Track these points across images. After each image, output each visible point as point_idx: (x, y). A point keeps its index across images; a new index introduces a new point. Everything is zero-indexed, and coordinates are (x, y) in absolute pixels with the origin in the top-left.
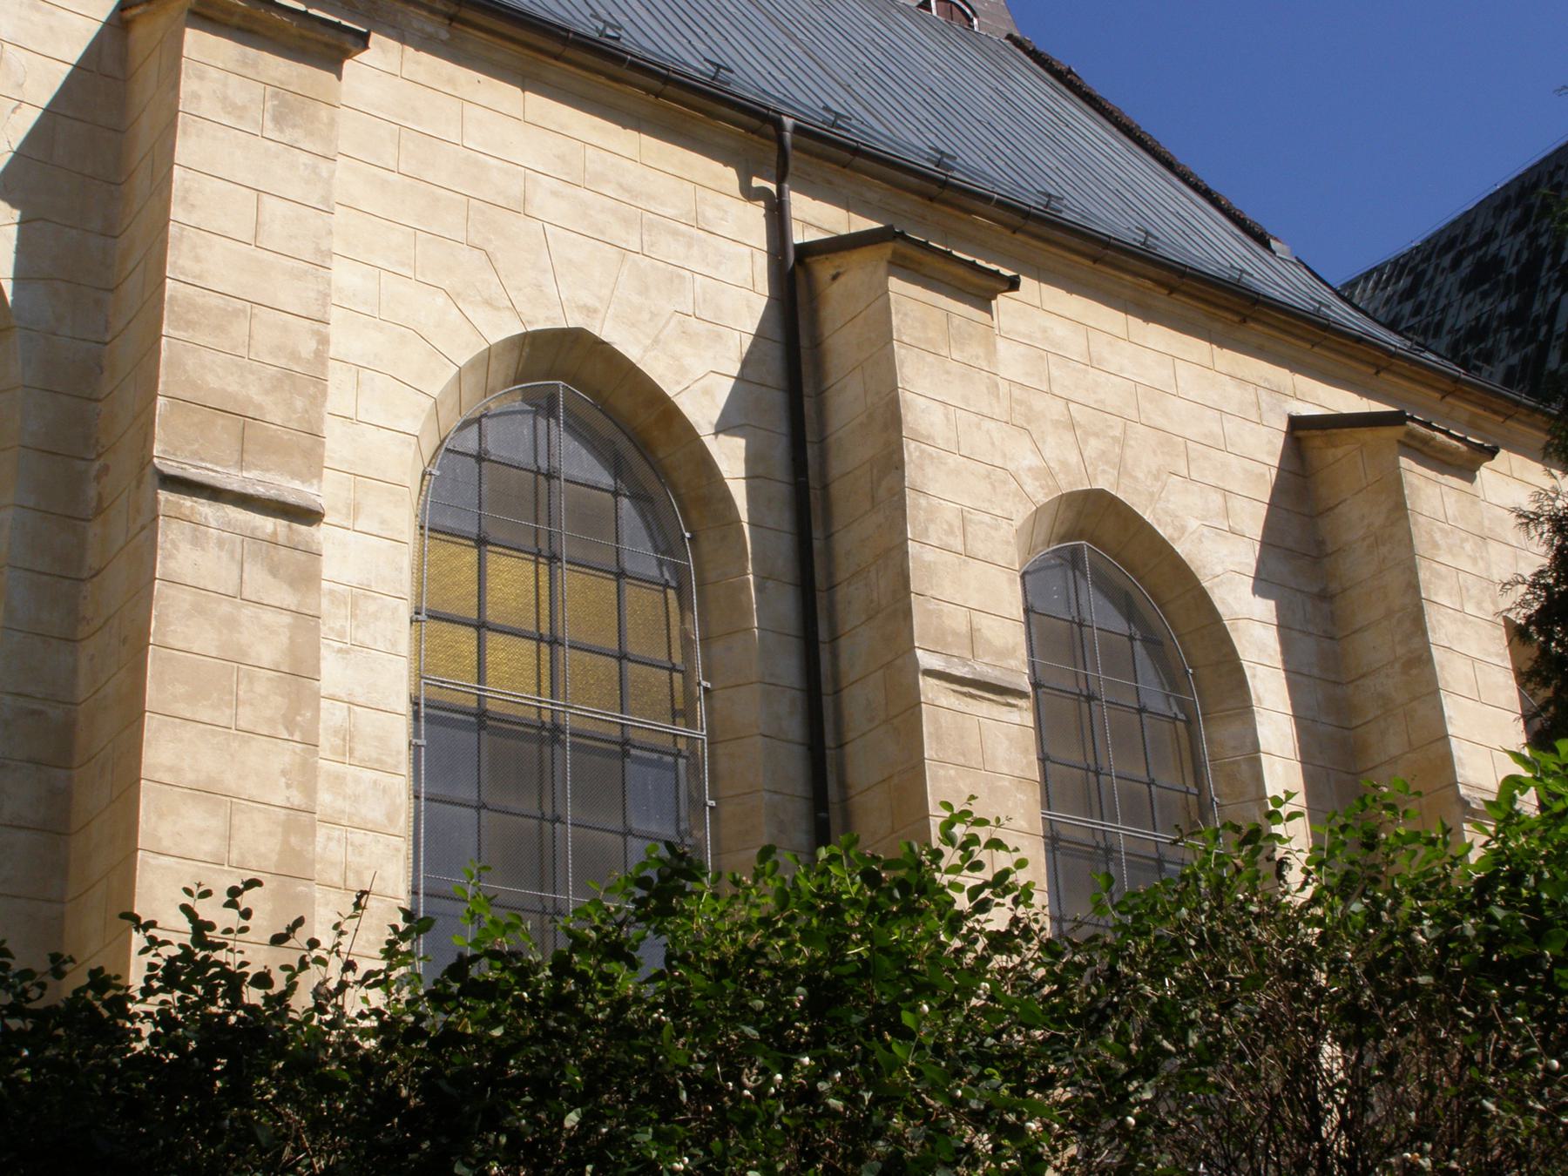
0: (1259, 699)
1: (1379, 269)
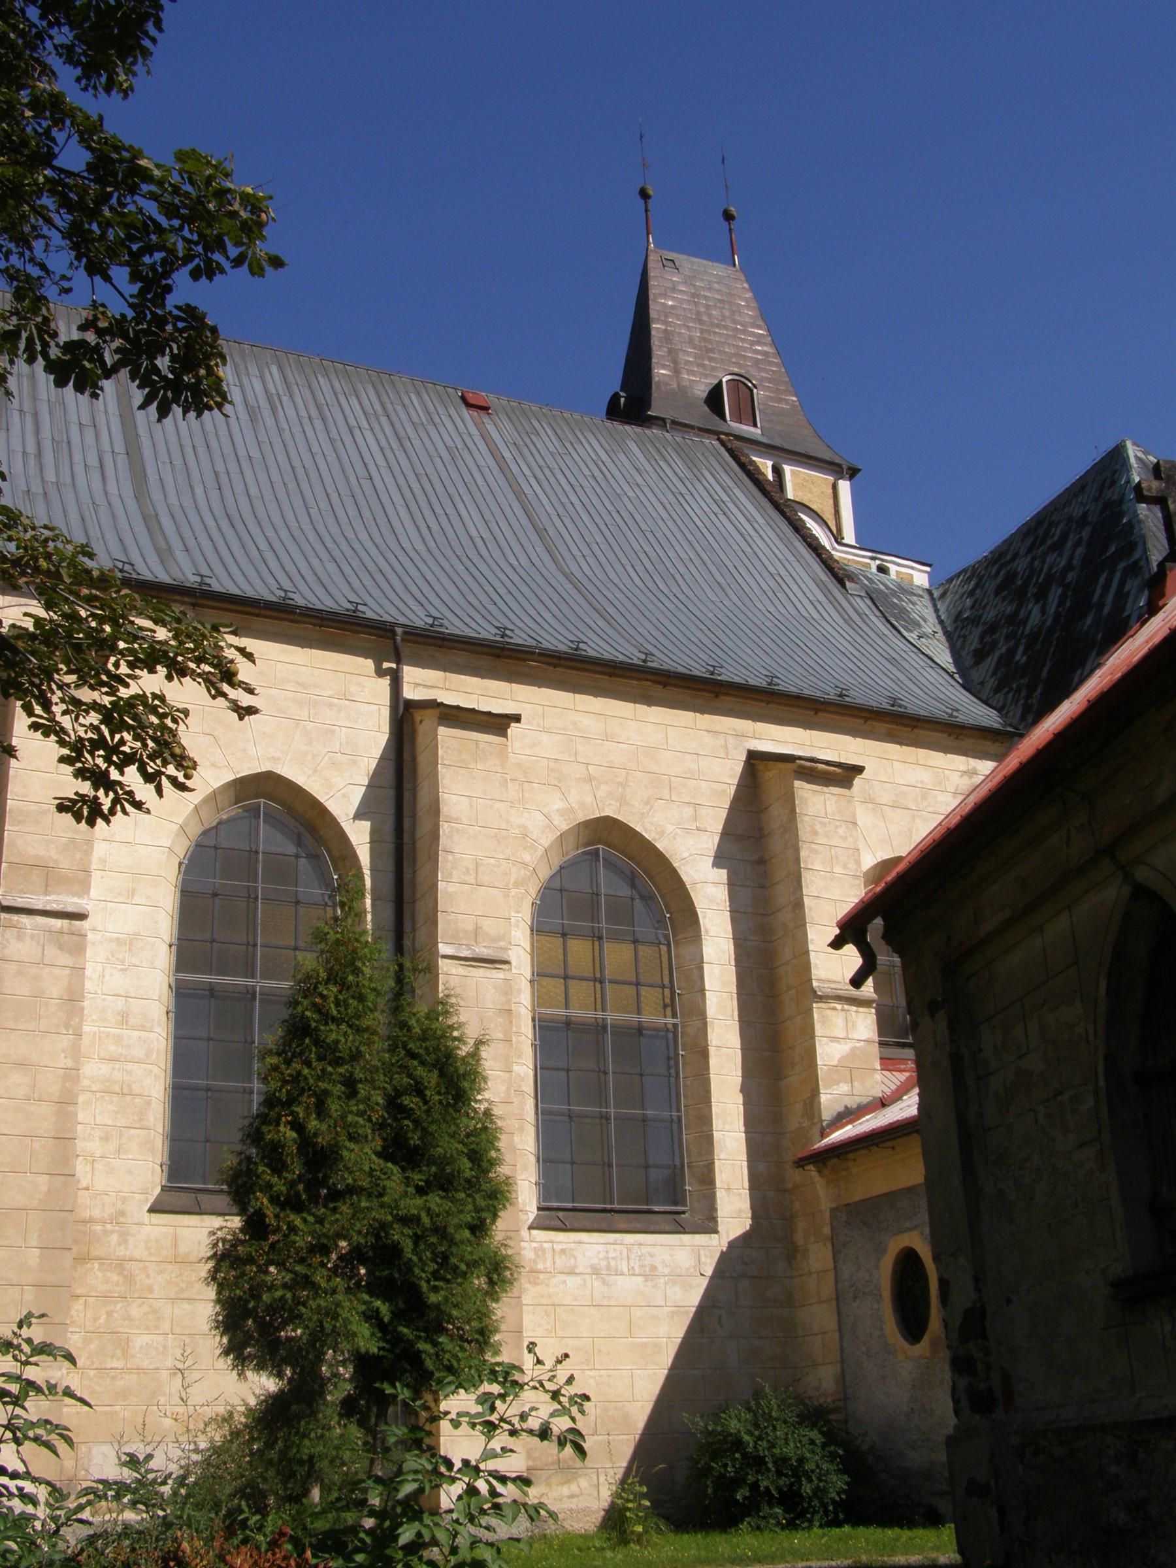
0: (707, 931)
1: (964, 571)
